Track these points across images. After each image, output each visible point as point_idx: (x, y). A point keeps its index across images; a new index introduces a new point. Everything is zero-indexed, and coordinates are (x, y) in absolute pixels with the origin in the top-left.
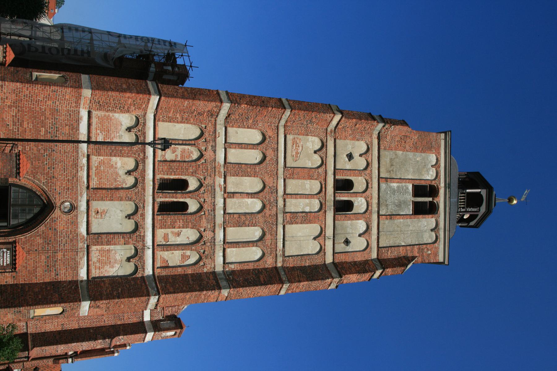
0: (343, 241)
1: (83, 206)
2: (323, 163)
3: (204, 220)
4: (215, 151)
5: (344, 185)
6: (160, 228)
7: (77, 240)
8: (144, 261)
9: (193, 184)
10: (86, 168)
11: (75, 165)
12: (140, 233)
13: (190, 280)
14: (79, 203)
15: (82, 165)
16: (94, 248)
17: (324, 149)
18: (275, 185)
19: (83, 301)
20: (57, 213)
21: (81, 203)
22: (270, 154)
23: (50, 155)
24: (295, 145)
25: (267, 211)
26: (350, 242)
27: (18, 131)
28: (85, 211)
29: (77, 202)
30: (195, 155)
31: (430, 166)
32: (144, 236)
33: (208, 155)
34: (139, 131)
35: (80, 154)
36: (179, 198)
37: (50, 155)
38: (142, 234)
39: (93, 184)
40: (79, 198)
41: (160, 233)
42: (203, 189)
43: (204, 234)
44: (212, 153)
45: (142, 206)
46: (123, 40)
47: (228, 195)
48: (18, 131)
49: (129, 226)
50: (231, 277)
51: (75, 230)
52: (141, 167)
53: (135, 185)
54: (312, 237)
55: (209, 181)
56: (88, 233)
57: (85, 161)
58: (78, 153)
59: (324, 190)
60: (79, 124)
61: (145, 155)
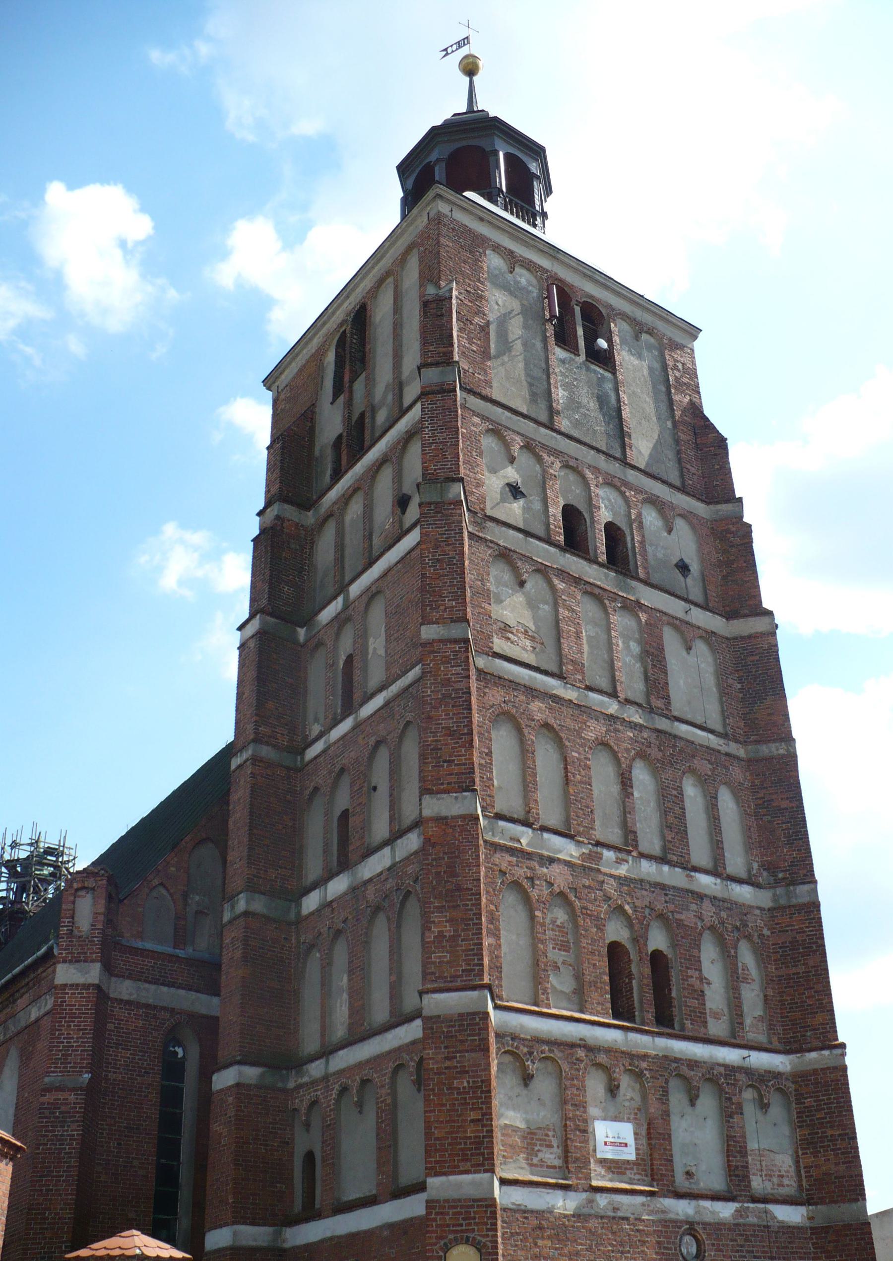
0: (682, 579)
2: (542, 570)
3: (683, 917)
4: (552, 860)
5: (574, 532)
6: (706, 1027)
7: (744, 1225)
8: (765, 1071)
9: (617, 931)
12: (721, 1074)
13: (794, 970)
14: (682, 1217)
15: (610, 1207)
16: (595, 1183)
21: (680, 1212)
24: (510, 635)
28: (694, 1203)
29: (681, 1222)
30: (560, 915)
31: (509, 277)
32: (726, 1066)
33: (560, 876)
34: (531, 1053)
36: (639, 972)
38: (722, 1070)
41: (717, 1028)
42: (627, 907)
43: (708, 922)
44: (556, 869)
45: (674, 1065)
50: (780, 875)
51: (730, 1229)
52: (602, 1058)
53: (638, 1075)
54: (684, 653)
55: (611, 887)
59: (597, 591)
61: (580, 1046)
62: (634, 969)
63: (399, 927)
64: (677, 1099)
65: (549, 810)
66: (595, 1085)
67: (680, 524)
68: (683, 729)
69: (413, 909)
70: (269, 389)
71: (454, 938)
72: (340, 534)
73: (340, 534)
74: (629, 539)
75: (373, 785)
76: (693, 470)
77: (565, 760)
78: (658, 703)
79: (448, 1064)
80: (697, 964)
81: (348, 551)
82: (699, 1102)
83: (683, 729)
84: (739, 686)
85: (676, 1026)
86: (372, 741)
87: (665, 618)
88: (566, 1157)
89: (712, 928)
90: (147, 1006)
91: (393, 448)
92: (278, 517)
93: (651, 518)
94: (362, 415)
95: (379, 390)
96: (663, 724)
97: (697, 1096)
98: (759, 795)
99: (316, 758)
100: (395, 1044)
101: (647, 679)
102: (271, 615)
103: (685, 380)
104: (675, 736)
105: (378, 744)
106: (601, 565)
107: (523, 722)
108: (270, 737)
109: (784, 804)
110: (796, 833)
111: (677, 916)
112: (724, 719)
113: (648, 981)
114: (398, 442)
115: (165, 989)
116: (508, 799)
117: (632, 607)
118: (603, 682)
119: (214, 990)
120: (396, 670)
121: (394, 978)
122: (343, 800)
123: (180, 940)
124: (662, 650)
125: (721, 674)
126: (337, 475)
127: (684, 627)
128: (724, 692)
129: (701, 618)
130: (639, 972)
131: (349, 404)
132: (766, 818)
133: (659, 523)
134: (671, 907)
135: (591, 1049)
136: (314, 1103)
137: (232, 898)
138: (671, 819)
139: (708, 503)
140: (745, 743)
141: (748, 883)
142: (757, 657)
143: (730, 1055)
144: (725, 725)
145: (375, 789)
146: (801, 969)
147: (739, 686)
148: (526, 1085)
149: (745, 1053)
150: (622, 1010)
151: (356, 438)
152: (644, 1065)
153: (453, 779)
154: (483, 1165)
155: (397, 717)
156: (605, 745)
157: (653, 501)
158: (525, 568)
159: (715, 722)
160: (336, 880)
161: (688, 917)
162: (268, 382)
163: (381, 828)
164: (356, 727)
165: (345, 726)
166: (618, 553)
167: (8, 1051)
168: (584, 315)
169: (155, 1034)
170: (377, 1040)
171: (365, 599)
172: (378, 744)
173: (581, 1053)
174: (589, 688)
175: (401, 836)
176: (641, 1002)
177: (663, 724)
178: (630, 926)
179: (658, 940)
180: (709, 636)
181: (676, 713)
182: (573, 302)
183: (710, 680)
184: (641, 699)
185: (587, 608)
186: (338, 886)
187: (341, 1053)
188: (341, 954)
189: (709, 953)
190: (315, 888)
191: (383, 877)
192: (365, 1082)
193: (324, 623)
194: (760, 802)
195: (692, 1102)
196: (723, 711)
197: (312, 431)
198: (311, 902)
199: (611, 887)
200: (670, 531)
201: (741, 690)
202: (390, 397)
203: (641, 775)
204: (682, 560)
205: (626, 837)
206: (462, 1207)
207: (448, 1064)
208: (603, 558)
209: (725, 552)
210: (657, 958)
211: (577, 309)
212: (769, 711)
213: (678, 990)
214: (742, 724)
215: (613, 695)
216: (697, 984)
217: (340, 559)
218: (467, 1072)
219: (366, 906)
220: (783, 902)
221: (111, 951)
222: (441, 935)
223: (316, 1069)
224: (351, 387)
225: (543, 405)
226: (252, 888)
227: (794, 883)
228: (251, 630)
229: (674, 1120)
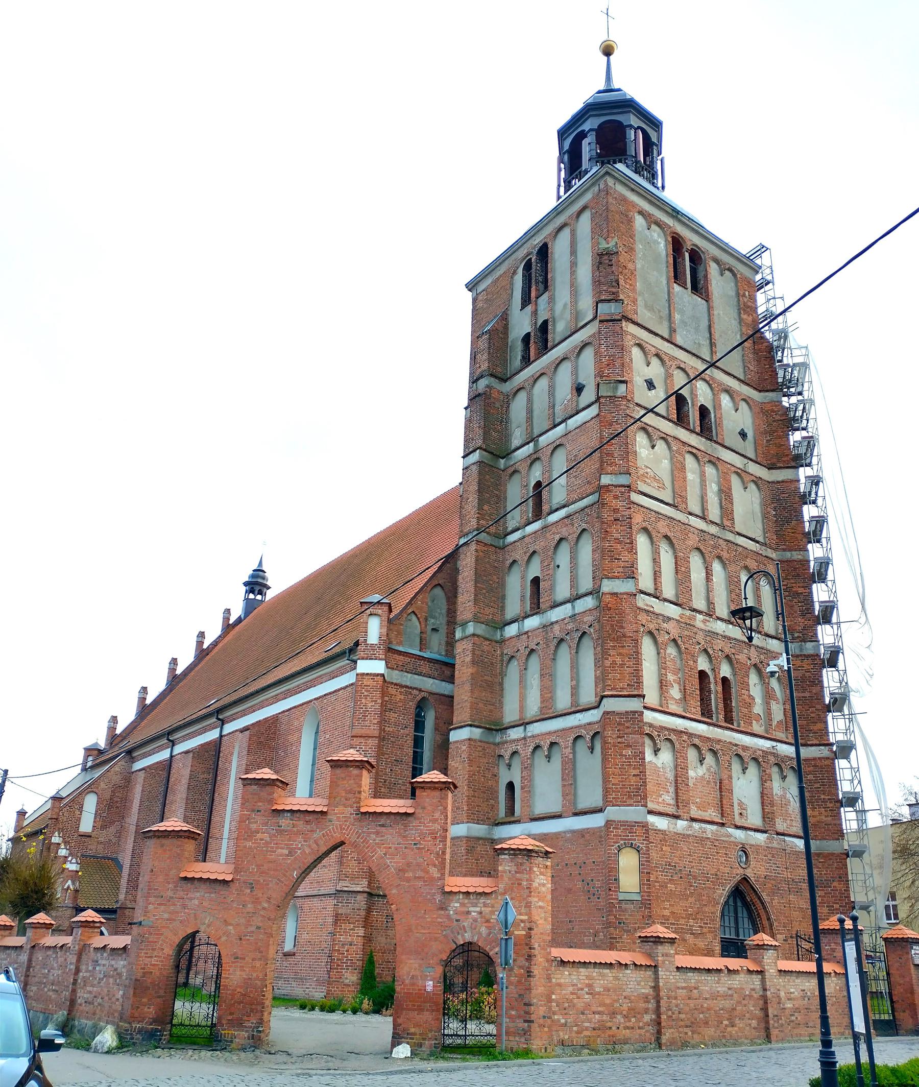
1: (739, 834)
9: (703, 664)
10: (703, 825)
11: (701, 840)
13: (803, 695)
17: (650, 429)
18: (696, 532)
19: (600, 827)
20: (749, 873)
22: (663, 527)
23: (695, 877)
25: (725, 555)
26: (739, 433)
27: (674, 924)
31: (647, 232)
34: (659, 736)
35: (690, 832)
36: (715, 688)
37: (695, 877)
39: (712, 814)
40: (732, 839)
41: (757, 728)
42: (709, 650)
43: (753, 661)
46: (818, 763)
47: (710, 613)
48: (674, 924)
49: (752, 770)
50: (796, 635)
52: (696, 741)
53: (714, 752)
54: (742, 490)
55: (700, 637)
56: (765, 832)
57: (696, 825)
58: (689, 836)
59: (694, 451)
60: (659, 830)
62: (712, 686)
64: (736, 767)
65: (669, 591)
66: (692, 754)
67: (743, 406)
68: (741, 541)
69: (587, 643)
70: (470, 290)
71: (622, 665)
72: (530, 400)
73: (530, 400)
74: (713, 415)
76: (752, 368)
77: (676, 557)
78: (727, 523)
79: (619, 740)
80: (746, 686)
81: (535, 413)
82: (747, 771)
83: (741, 541)
85: (735, 724)
86: (557, 537)
87: (733, 468)
88: (677, 799)
89: (755, 665)
90: (407, 687)
91: (572, 351)
92: (487, 386)
93: (725, 400)
94: (545, 322)
95: (559, 307)
96: (730, 537)
97: (747, 768)
99: (515, 542)
100: (576, 723)
101: (721, 507)
102: (485, 450)
103: (750, 304)
104: (737, 545)
105: (561, 539)
106: (698, 434)
107: (654, 534)
109: (800, 590)
110: (807, 609)
111: (737, 656)
112: (765, 533)
113: (720, 695)
114: (576, 347)
115: (416, 676)
116: (646, 581)
117: (714, 462)
118: (697, 510)
119: (451, 679)
121: (574, 682)
122: (535, 570)
123: (423, 645)
124: (730, 489)
125: (764, 505)
126: (527, 361)
127: (743, 474)
128: (765, 516)
129: (753, 468)
130: (715, 688)
131: (535, 313)
133: (730, 405)
134: (733, 651)
135: (691, 735)
136: (515, 753)
137: (464, 624)
138: (734, 596)
139: (760, 391)
140: (775, 550)
141: (776, 638)
143: (766, 744)
144: (765, 538)
145: (558, 566)
146: (807, 694)
148: (656, 755)
149: (774, 744)
150: (706, 713)
151: (541, 338)
152: (718, 747)
153: (621, 570)
155: (576, 525)
156: (698, 549)
157: (728, 391)
158: (747, 478)
159: (759, 535)
160: (531, 618)
161: (742, 657)
162: (471, 286)
163: (563, 590)
164: (545, 527)
165: (536, 526)
166: (706, 424)
168: (690, 260)
169: (411, 703)
170: (560, 720)
171: (552, 447)
173: (685, 737)
174: (691, 514)
175: (579, 598)
176: (717, 708)
177: (730, 537)
178: (711, 661)
179: (725, 670)
180: (757, 481)
181: (737, 530)
182: (684, 249)
183: (757, 508)
184: (718, 521)
185: (690, 461)
186: (532, 623)
189: (753, 678)
190: (514, 622)
191: (566, 621)
192: (552, 744)
193: (520, 458)
195: (744, 770)
196: (764, 529)
197: (506, 328)
198: (511, 630)
199: (700, 637)
200: (736, 410)
201: (775, 516)
202: (568, 312)
204: (742, 430)
205: (709, 607)
207: (619, 740)
208: (698, 429)
210: (725, 680)
211: (687, 255)
213: (736, 702)
214: (775, 537)
215: (703, 518)
216: (748, 700)
217: (530, 418)
218: (631, 746)
219: (557, 640)
221: (389, 651)
222: (614, 662)
223: (515, 734)
224: (536, 301)
225: (666, 324)
226: (476, 620)
227: (804, 641)
228: (475, 457)
229: (734, 780)
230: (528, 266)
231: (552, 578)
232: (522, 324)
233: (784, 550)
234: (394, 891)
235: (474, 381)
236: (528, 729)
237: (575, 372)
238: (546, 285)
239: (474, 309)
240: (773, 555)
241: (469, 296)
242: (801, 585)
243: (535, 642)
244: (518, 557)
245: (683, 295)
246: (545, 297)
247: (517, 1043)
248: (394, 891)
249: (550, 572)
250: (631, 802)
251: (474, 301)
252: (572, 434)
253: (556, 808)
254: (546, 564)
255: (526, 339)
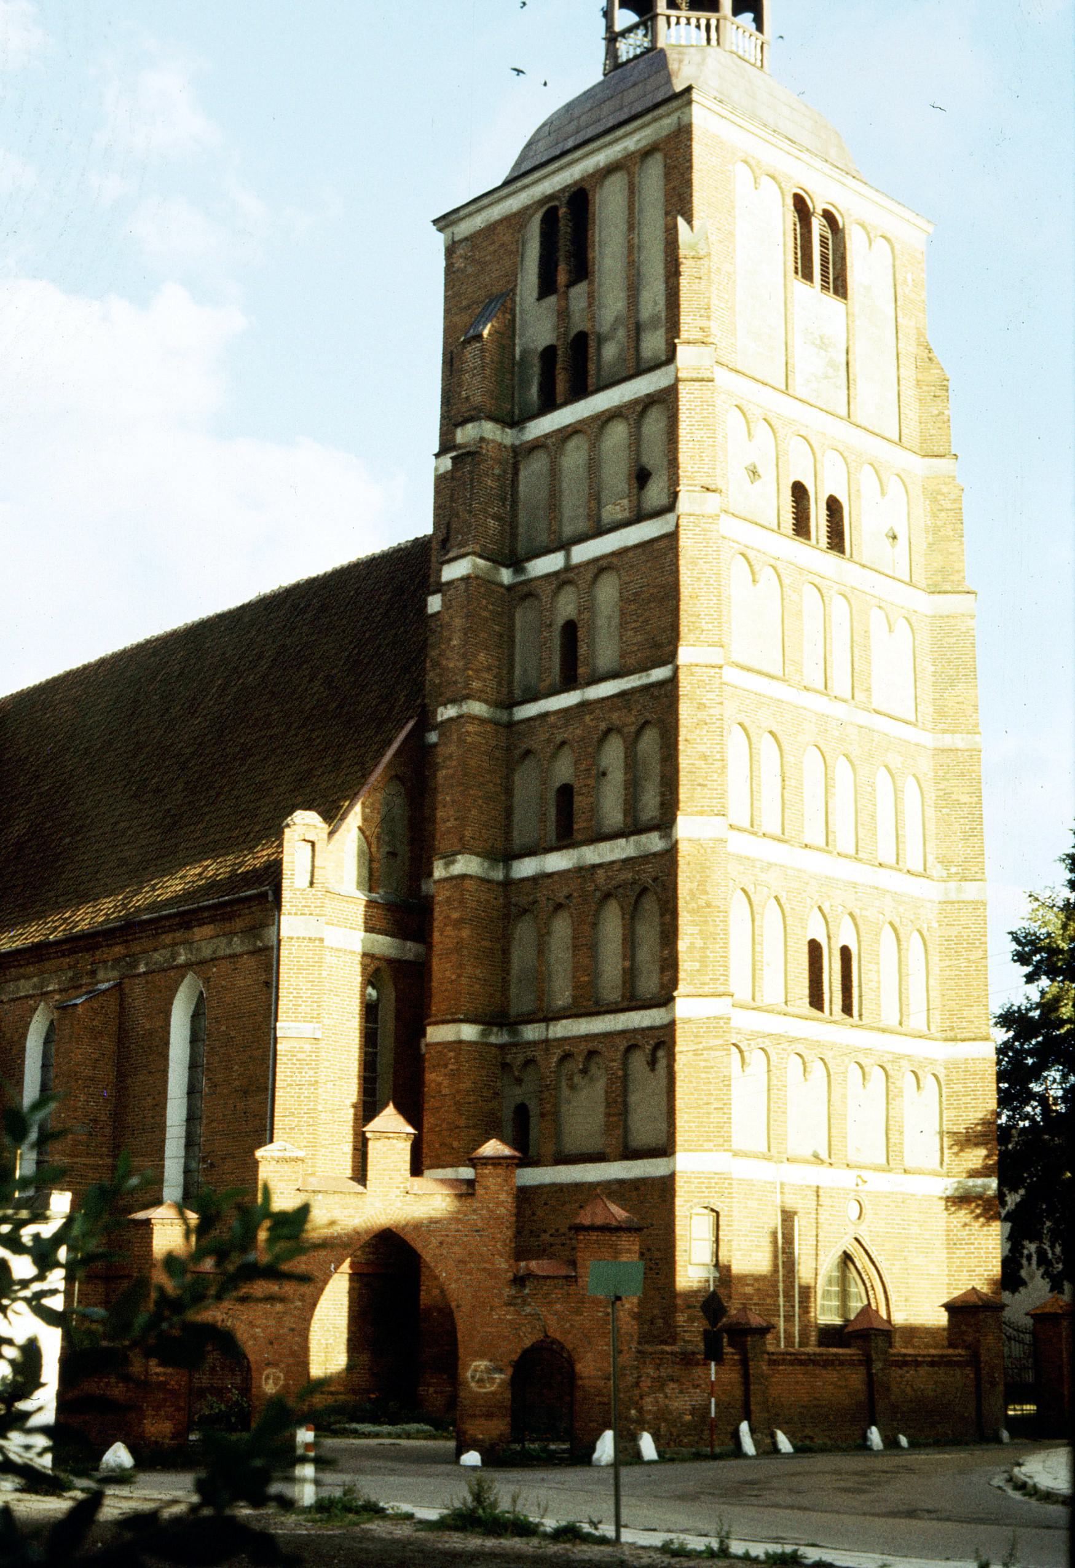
50: (953, 870)
59: (817, 580)
63: (633, 918)
65: (771, 823)
70: (440, 230)
75: (601, 769)
84: (933, 668)
86: (603, 726)
98: (941, 787)
105: (608, 732)
108: (482, 691)
109: (964, 799)
111: (864, 913)
116: (739, 813)
120: (631, 661)
122: (564, 771)
132: (944, 811)
142: (953, 640)
145: (604, 774)
147: (933, 668)
154: (723, 1145)
167: (183, 977)
172: (608, 732)
177: (863, 718)
187: (564, 1021)
188: (562, 928)
194: (941, 793)
203: (842, 769)
206: (706, 1178)
209: (935, 516)
212: (960, 699)
220: (953, 897)
224: (566, 293)
230: (550, 220)
231: (595, 791)
232: (538, 327)
233: (944, 731)
234: (453, 1286)
235: (454, 415)
236: (551, 1028)
237: (636, 440)
238: (582, 270)
239: (449, 270)
240: (928, 739)
241: (438, 241)
242: (965, 790)
243: (566, 891)
244: (535, 746)
245: (811, 296)
246: (581, 288)
247: (978, 876)
248: (453, 1286)
249: (591, 782)
250: (710, 1145)
251: (450, 251)
252: (630, 554)
253: (595, 1144)
254: (583, 767)
255: (549, 354)
